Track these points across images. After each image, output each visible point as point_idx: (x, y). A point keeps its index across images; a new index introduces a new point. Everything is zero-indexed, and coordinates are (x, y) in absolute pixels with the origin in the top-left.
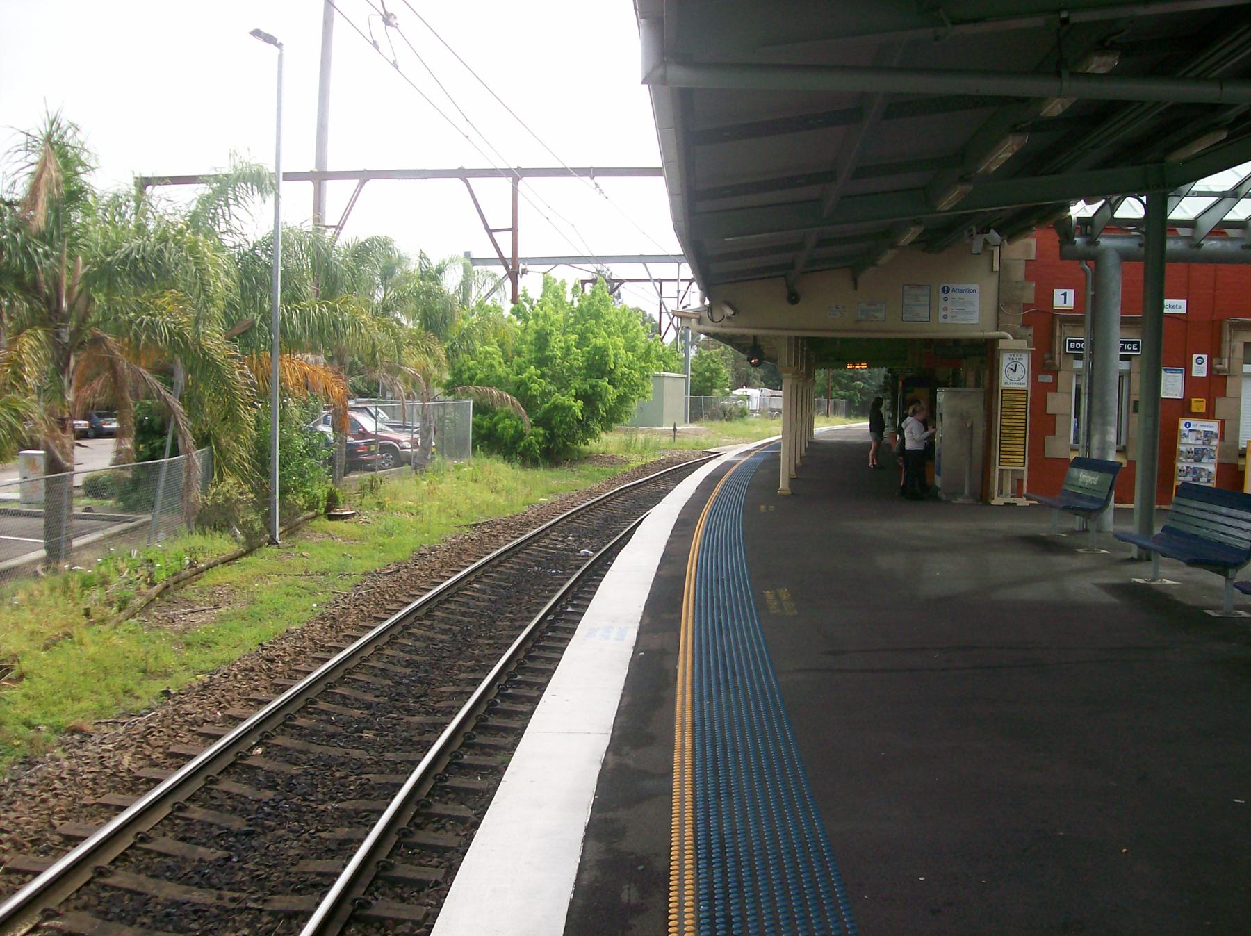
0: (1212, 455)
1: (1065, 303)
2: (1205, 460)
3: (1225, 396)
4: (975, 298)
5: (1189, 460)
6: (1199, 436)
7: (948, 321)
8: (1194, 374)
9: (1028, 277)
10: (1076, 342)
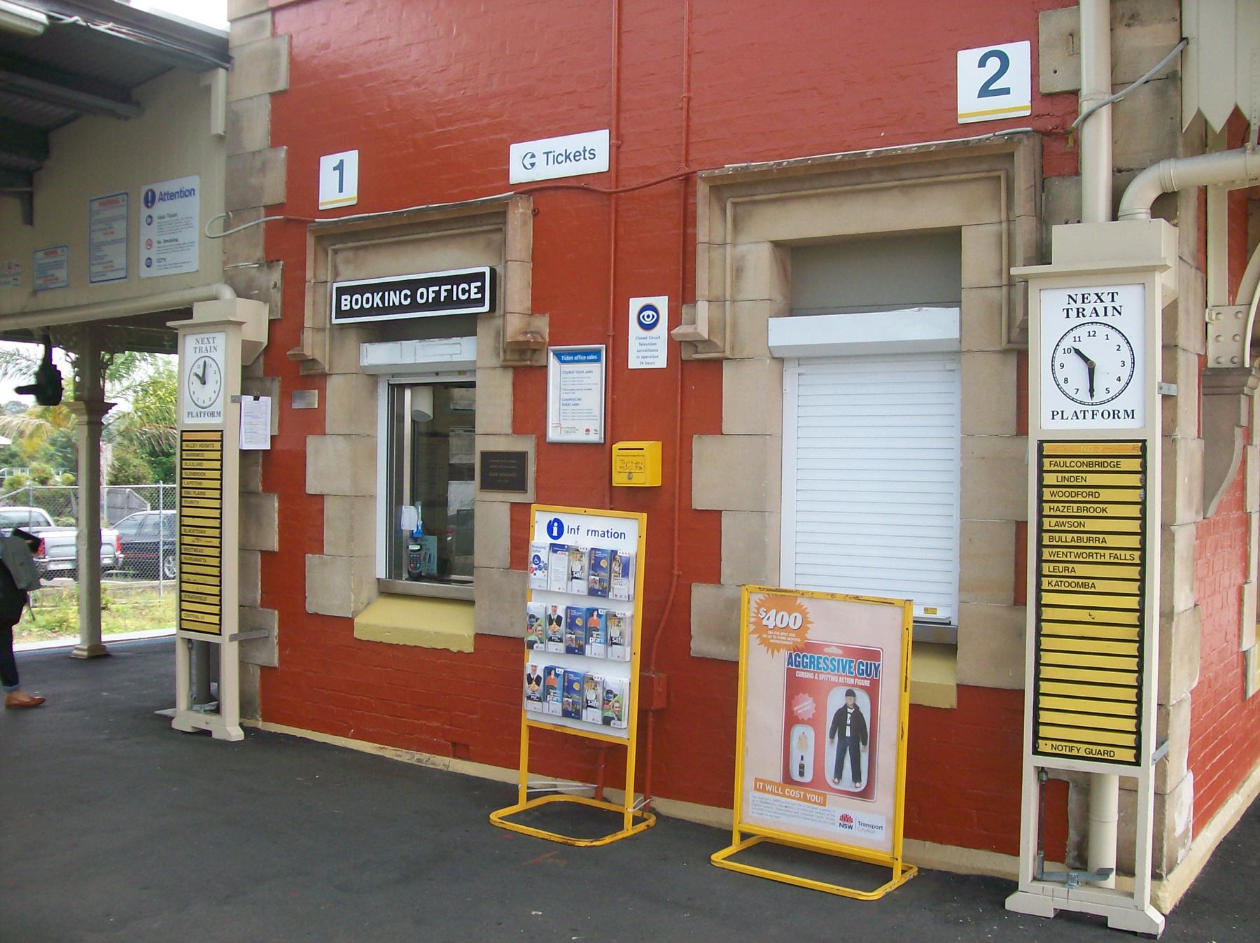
0: (614, 632)
1: (341, 190)
2: (595, 647)
3: (325, 434)
4: (191, 208)
5: (552, 646)
6: (576, 567)
7: (154, 272)
8: (634, 363)
9: (276, 142)
10: (351, 291)
